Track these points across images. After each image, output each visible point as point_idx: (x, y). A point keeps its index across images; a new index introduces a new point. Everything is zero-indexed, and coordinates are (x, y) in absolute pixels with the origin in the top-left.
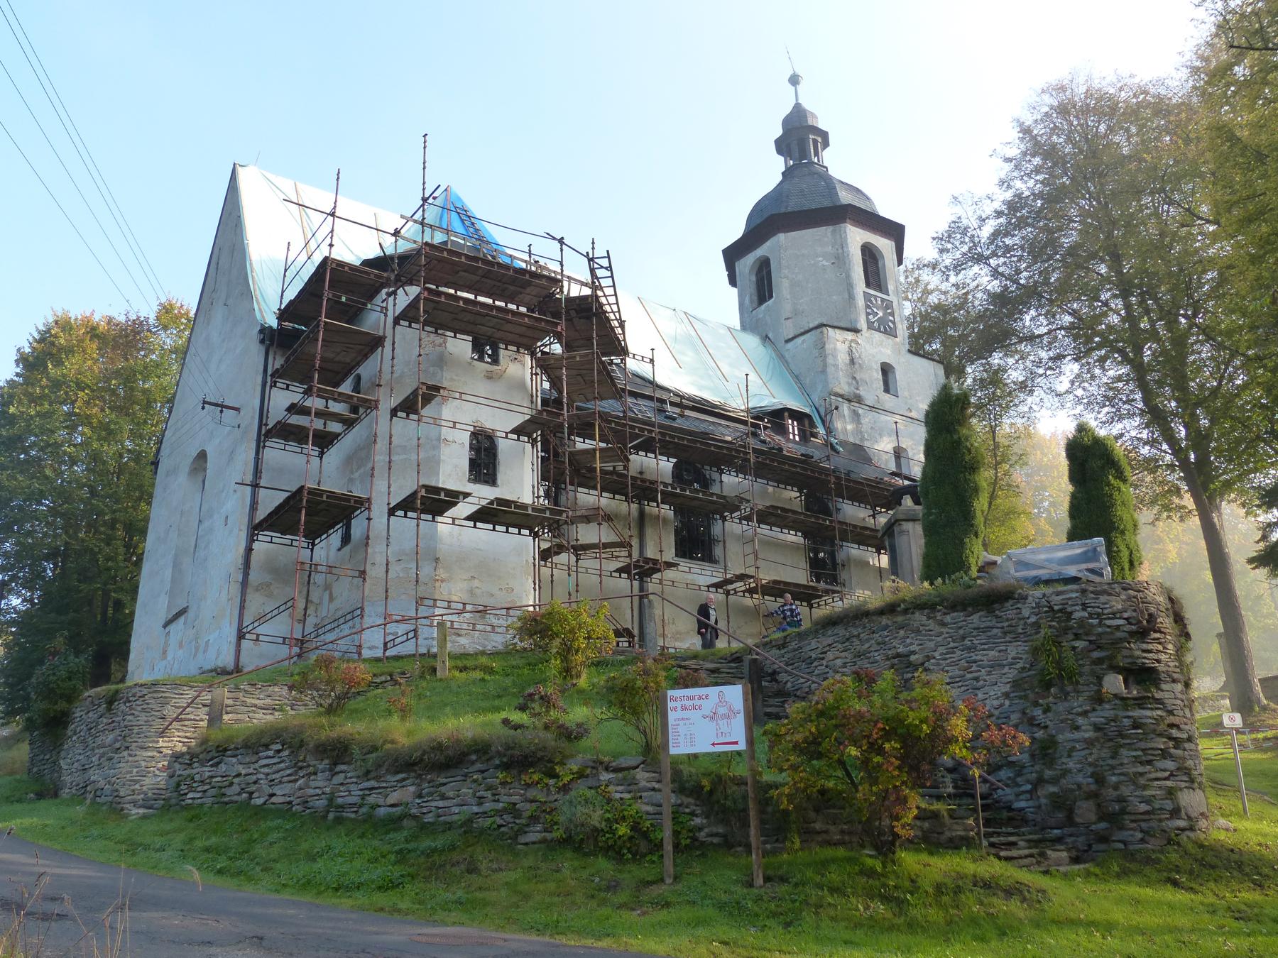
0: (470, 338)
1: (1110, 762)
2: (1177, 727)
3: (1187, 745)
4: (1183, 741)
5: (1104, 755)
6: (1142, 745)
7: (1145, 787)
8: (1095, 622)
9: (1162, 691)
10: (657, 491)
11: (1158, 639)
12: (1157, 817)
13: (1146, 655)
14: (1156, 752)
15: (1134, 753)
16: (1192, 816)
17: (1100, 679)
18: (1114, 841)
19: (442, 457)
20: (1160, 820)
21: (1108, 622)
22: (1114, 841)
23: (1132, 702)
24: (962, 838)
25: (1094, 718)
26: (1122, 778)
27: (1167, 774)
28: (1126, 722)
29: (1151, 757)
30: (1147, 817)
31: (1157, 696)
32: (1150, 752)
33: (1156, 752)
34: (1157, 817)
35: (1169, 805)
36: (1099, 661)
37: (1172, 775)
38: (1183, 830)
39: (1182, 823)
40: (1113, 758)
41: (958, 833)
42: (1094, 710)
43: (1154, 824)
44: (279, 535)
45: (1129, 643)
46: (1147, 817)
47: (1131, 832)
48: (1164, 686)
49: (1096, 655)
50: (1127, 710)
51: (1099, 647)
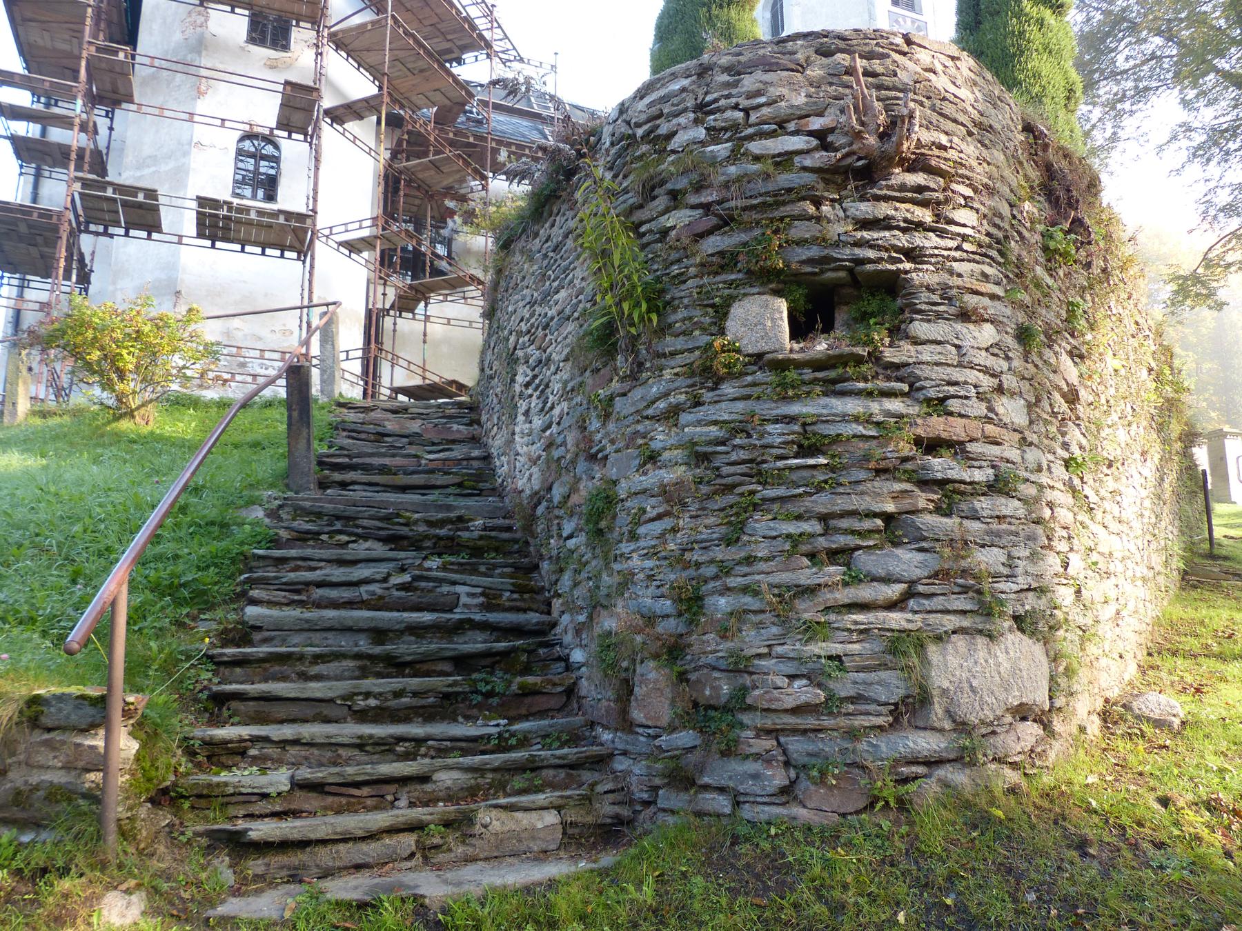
0: (247, 12)
1: (720, 553)
2: (955, 447)
3: (983, 505)
4: (975, 490)
5: (705, 534)
6: (822, 503)
7: (811, 631)
8: (721, 149)
9: (916, 342)
10: (79, 58)
11: (920, 189)
12: (842, 722)
13: (866, 235)
14: (867, 524)
15: (792, 528)
16: (973, 719)
17: (721, 312)
18: (706, 788)
19: (193, 165)
20: (852, 734)
21: (755, 147)
22: (706, 788)
23: (808, 374)
24: (56, 794)
25: (695, 427)
26: (748, 601)
27: (895, 591)
28: (776, 433)
29: (842, 540)
30: (810, 722)
31: (889, 355)
32: (844, 523)
33: (867, 524)
34: (842, 722)
35: (890, 685)
36: (726, 261)
37: (909, 594)
38: (932, 763)
39: (925, 743)
40: (729, 542)
41: (47, 776)
42: (698, 403)
43: (830, 746)
44: (38, 279)
45: (817, 203)
46: (810, 722)
47: (752, 767)
48: (920, 328)
49: (713, 244)
50: (785, 399)
51: (726, 222)
